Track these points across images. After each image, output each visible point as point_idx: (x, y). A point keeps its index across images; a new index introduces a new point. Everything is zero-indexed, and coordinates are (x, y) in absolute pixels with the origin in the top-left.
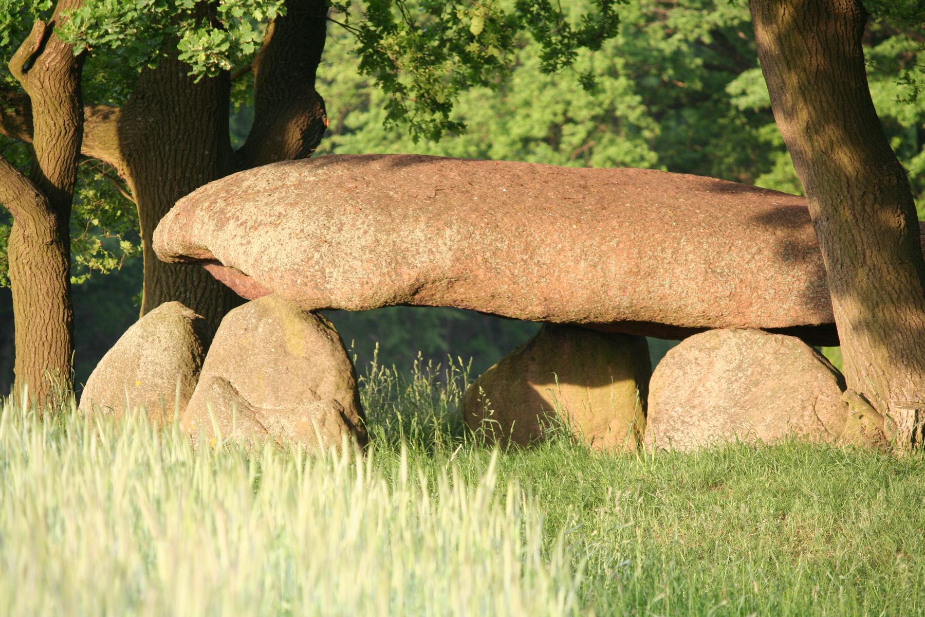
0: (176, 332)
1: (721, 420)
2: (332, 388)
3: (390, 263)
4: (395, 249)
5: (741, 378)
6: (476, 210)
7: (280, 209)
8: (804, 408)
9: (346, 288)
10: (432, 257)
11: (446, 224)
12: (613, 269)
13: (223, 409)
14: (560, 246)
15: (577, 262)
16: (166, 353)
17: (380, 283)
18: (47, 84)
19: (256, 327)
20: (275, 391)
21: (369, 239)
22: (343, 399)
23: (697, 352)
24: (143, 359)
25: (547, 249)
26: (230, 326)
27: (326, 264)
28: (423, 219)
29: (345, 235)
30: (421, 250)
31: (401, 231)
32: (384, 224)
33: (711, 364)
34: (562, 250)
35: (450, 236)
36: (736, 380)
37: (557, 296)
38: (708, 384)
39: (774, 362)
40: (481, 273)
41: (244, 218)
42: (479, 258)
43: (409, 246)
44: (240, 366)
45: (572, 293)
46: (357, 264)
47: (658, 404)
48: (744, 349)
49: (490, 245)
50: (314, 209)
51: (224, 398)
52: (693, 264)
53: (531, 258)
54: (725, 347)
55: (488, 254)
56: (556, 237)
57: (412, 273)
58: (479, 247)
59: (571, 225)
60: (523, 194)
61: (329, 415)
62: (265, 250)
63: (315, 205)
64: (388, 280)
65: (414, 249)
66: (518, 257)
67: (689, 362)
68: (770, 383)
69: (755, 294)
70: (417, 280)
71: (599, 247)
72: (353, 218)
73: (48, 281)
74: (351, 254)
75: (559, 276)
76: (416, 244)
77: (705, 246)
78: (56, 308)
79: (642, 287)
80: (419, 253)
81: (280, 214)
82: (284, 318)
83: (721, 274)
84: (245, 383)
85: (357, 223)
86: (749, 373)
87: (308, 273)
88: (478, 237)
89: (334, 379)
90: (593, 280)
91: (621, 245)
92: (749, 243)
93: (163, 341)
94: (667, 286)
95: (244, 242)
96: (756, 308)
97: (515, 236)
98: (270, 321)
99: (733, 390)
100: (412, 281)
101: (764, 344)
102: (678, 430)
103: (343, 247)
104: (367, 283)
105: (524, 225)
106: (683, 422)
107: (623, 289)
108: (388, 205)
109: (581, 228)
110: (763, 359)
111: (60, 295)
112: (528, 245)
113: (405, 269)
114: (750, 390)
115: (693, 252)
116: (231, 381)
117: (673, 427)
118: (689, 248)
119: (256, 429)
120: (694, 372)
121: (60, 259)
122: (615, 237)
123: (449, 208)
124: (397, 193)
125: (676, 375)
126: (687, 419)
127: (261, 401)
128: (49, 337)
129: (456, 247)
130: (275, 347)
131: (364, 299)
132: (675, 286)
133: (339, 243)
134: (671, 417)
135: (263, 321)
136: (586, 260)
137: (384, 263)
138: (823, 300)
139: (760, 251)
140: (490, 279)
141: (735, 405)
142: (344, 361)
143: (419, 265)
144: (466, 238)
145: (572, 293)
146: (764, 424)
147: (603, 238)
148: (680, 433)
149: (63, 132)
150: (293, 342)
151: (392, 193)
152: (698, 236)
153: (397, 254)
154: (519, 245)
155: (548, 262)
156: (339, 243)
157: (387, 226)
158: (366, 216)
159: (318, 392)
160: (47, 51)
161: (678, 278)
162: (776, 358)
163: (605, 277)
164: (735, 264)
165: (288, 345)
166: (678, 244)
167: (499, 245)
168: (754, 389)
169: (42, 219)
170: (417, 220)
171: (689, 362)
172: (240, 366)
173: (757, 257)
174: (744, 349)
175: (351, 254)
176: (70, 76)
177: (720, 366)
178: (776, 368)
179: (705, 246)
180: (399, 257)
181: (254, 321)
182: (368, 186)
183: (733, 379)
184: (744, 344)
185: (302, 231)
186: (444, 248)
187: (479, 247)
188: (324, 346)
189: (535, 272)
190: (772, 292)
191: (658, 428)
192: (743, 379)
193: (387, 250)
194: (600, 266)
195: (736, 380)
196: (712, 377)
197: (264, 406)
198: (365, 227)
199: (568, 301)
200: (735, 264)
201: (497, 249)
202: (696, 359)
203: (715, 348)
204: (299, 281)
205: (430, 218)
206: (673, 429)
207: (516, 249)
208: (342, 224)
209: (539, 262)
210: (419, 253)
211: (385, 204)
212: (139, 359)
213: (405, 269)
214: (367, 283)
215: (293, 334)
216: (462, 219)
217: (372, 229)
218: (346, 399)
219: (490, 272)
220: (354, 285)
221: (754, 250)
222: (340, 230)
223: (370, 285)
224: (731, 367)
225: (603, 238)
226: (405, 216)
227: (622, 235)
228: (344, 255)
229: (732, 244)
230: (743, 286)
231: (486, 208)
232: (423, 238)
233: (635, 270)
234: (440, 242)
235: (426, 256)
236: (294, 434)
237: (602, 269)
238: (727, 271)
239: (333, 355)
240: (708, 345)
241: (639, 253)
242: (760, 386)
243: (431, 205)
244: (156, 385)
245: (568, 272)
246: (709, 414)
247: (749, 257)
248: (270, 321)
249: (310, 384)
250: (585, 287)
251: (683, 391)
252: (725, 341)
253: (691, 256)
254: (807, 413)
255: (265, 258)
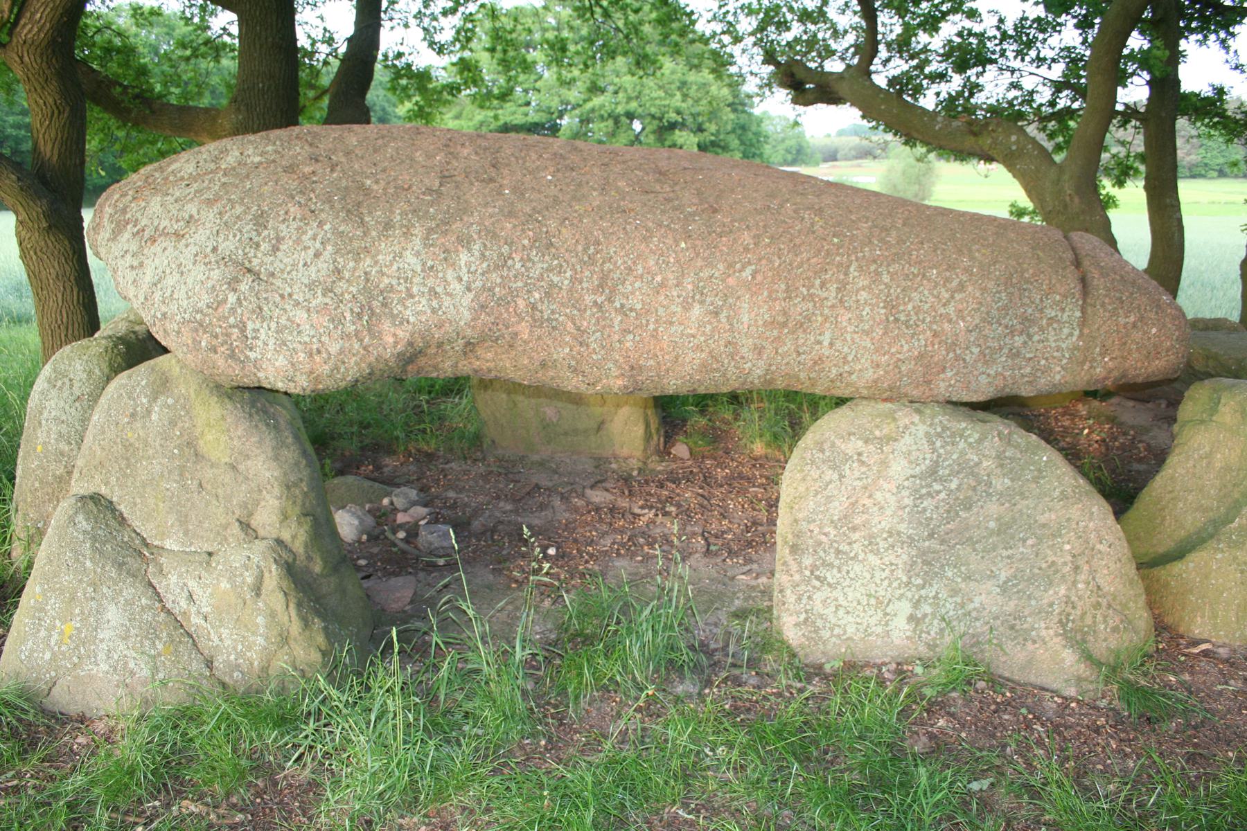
0: (97, 371)
1: (905, 557)
2: (275, 519)
3: (359, 316)
4: (369, 288)
5: (939, 492)
6: (511, 214)
7: (192, 209)
8: (1077, 568)
9: (281, 361)
10: (435, 304)
11: (460, 240)
12: (745, 319)
13: (88, 564)
14: (659, 278)
15: (687, 307)
16: (77, 404)
17: (341, 352)
18: (26, 59)
19: (149, 412)
20: (183, 520)
21: (321, 268)
22: (294, 537)
23: (860, 443)
24: (45, 414)
25: (637, 285)
26: (109, 409)
27: (246, 315)
28: (418, 231)
29: (285, 258)
30: (415, 290)
31: (379, 252)
32: (351, 240)
33: (884, 464)
34: (662, 285)
35: (468, 265)
36: (929, 494)
37: (651, 362)
38: (878, 496)
39: (998, 471)
40: (524, 329)
41: (144, 222)
42: (521, 303)
43: (394, 282)
44: (125, 475)
45: (677, 358)
46: (300, 315)
47: (796, 521)
48: (938, 444)
49: (541, 278)
50: (239, 210)
51: (94, 539)
52: (867, 309)
53: (610, 300)
54: (907, 439)
55: (537, 296)
56: (652, 263)
57: (401, 334)
58: (520, 284)
59: (677, 243)
60: (580, 185)
61: (267, 575)
62: (159, 281)
63: (242, 203)
64: (356, 346)
65: (402, 288)
66: (588, 299)
67: (848, 458)
68: (993, 508)
69: (951, 355)
70: (411, 344)
71: (723, 281)
72: (299, 228)
73: (56, 265)
74: (290, 295)
75: (656, 330)
76: (406, 280)
77: (886, 278)
78: (68, 291)
79: (788, 346)
80: (412, 296)
81: (191, 217)
82: (193, 395)
83: (906, 323)
84: (135, 505)
85: (304, 238)
86: (953, 486)
87: (218, 330)
88: (518, 266)
89: (277, 502)
90: (712, 337)
91: (759, 278)
92: (948, 274)
93: (76, 384)
94: (826, 343)
95: (135, 263)
96: (949, 374)
97: (581, 261)
98: (170, 401)
99: (925, 510)
100: (399, 348)
101: (980, 441)
102: (831, 565)
103: (278, 282)
104: (319, 352)
105: (598, 243)
106: (838, 552)
107: (759, 351)
108: (359, 204)
109: (694, 247)
110: (977, 464)
111: (72, 278)
112: (604, 278)
113: (386, 325)
114: (957, 514)
115: (869, 288)
116: (115, 499)
117: (824, 561)
118: (863, 282)
119: (144, 601)
120: (857, 474)
121: (66, 242)
122: (749, 263)
123: (465, 210)
124: (377, 182)
125: (827, 478)
126: (844, 547)
127: (163, 535)
128: (65, 320)
129: (479, 284)
130: (179, 447)
131: (316, 379)
132: (838, 344)
133: (273, 274)
134: (820, 543)
135: (159, 402)
136: (702, 302)
137: (348, 315)
138: (1043, 362)
139: (961, 287)
140: (539, 338)
141: (931, 536)
142: (297, 464)
143: (412, 319)
144: (497, 267)
145: (677, 358)
146: (994, 582)
147: (731, 265)
148: (835, 571)
149: (56, 112)
150: (209, 437)
151: (368, 182)
152: (874, 261)
153: (372, 298)
154: (589, 279)
155: (639, 306)
156: (273, 274)
157: (356, 244)
158: (321, 224)
159: (254, 524)
160: (22, 22)
161: (843, 331)
162: (1001, 466)
163: (732, 330)
164: (927, 306)
165: (201, 442)
166: (846, 274)
167: (556, 279)
168: (963, 514)
169: (31, 203)
170: (407, 234)
171: (848, 458)
172: (125, 475)
173: (958, 296)
174: (938, 444)
175: (290, 295)
176: (53, 51)
177: (899, 468)
178: (1001, 483)
179: (886, 278)
180: (375, 304)
181: (144, 401)
182: (332, 170)
183: (924, 491)
184: (939, 435)
185: (215, 249)
186: (456, 287)
187: (520, 284)
188: (261, 442)
189: (616, 323)
190: (976, 350)
191: (800, 563)
192: (943, 495)
193: (354, 290)
194: (724, 314)
195: (929, 494)
196: (886, 486)
197: (169, 544)
198: (318, 245)
199: (667, 371)
200: (927, 306)
201: (552, 285)
202: (860, 454)
203: (890, 439)
204: (203, 344)
205: (430, 231)
206: (825, 564)
207: (585, 285)
208: (279, 239)
209: (622, 306)
210: (412, 296)
211: (354, 203)
212: (41, 414)
213: (386, 325)
214: (319, 352)
215: (208, 425)
216: (488, 232)
217: (329, 248)
218: (297, 535)
219: (541, 327)
220: (303, 346)
221: (955, 284)
222: (275, 249)
223: (324, 355)
224: (918, 470)
225: (731, 265)
226: (388, 225)
227: (760, 260)
228: (278, 299)
229: (924, 276)
230: (936, 341)
231: (528, 210)
232: (419, 269)
233: (781, 319)
234: (450, 275)
235: (424, 301)
236: (209, 609)
237: (728, 317)
238: (914, 318)
239: (276, 458)
240: (877, 433)
241: (787, 290)
242: (975, 510)
243: (432, 204)
244: (62, 454)
245: (671, 323)
246: (882, 544)
247: (947, 296)
248: (170, 401)
249: (237, 512)
250: (698, 348)
251: (837, 504)
252: (906, 427)
253: (864, 295)
254: (1083, 577)
255: (157, 296)
